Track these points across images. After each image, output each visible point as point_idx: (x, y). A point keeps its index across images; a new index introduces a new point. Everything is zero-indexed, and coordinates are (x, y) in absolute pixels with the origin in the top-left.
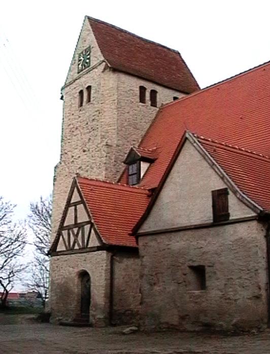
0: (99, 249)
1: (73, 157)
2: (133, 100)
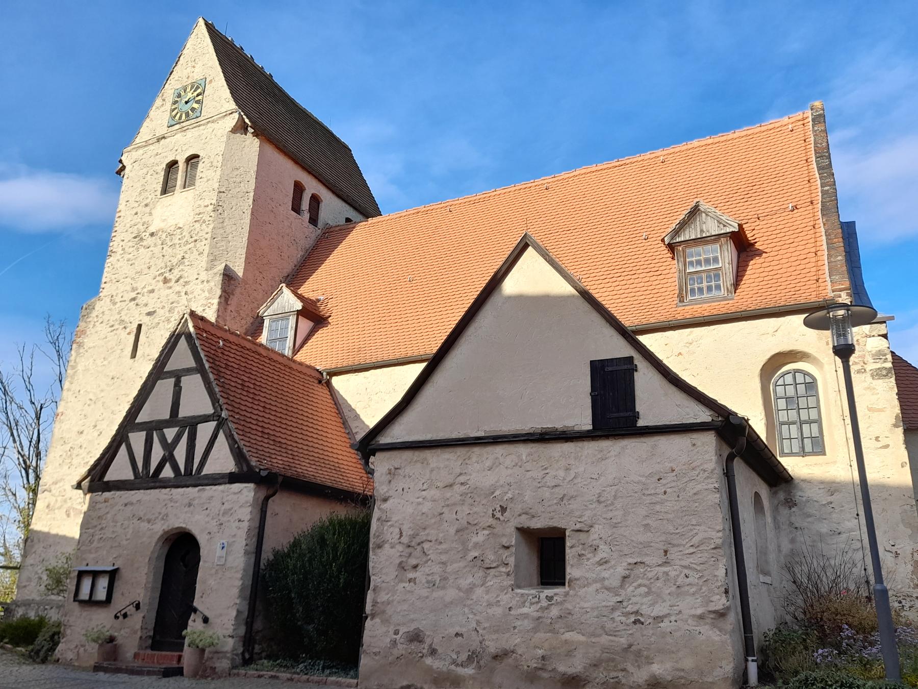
0: (232, 478)
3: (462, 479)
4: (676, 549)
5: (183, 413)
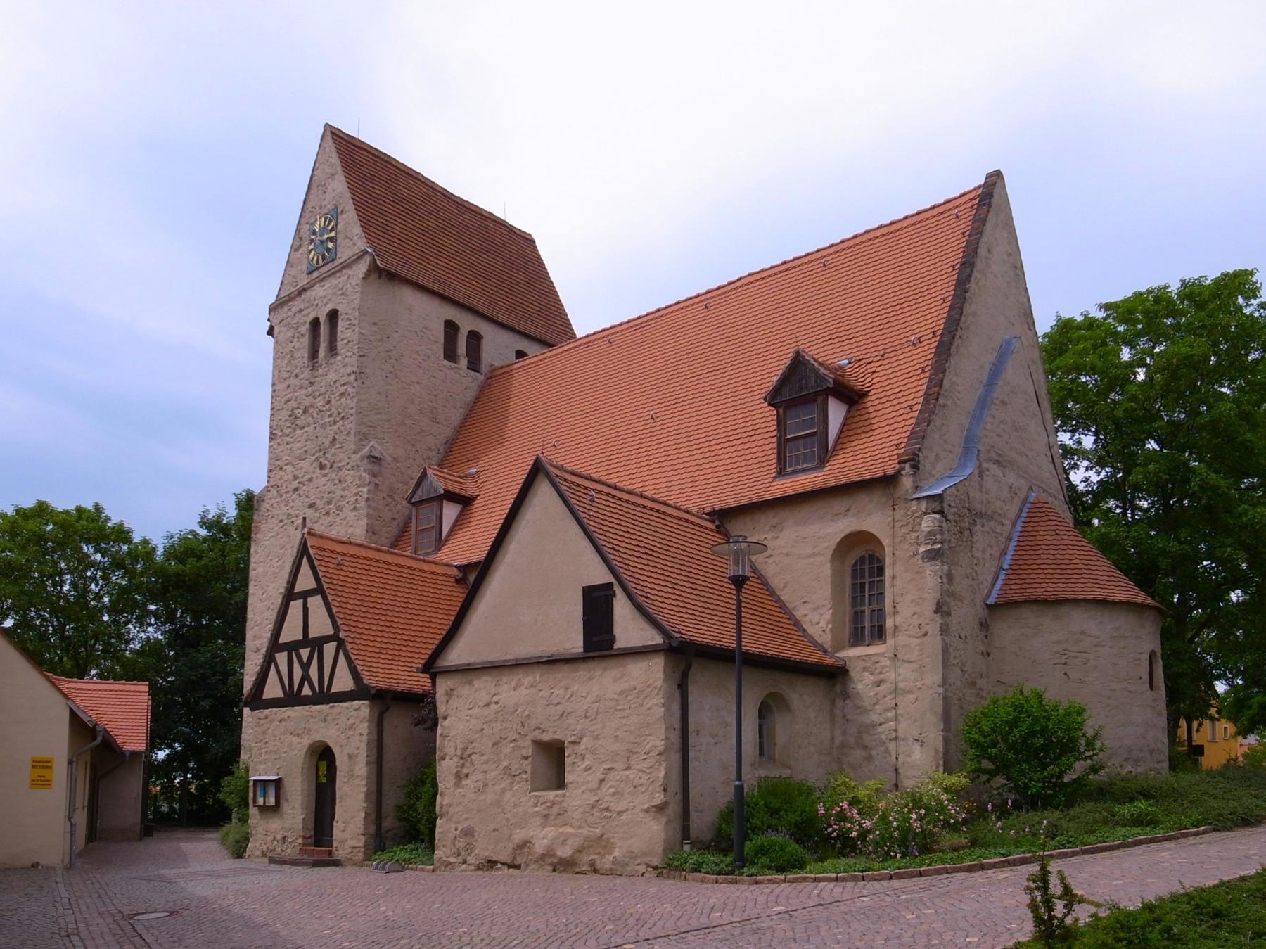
1: (295, 478)
2: (430, 353)
3: (495, 699)
4: (635, 756)
5: (313, 633)
